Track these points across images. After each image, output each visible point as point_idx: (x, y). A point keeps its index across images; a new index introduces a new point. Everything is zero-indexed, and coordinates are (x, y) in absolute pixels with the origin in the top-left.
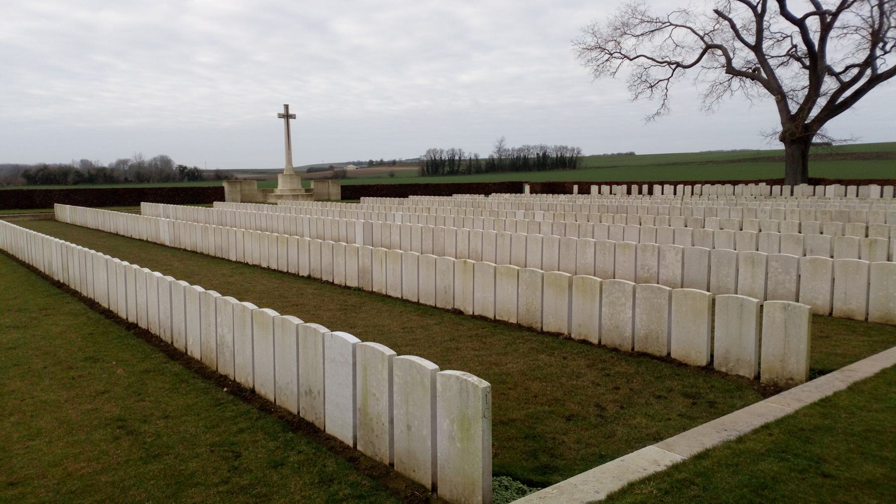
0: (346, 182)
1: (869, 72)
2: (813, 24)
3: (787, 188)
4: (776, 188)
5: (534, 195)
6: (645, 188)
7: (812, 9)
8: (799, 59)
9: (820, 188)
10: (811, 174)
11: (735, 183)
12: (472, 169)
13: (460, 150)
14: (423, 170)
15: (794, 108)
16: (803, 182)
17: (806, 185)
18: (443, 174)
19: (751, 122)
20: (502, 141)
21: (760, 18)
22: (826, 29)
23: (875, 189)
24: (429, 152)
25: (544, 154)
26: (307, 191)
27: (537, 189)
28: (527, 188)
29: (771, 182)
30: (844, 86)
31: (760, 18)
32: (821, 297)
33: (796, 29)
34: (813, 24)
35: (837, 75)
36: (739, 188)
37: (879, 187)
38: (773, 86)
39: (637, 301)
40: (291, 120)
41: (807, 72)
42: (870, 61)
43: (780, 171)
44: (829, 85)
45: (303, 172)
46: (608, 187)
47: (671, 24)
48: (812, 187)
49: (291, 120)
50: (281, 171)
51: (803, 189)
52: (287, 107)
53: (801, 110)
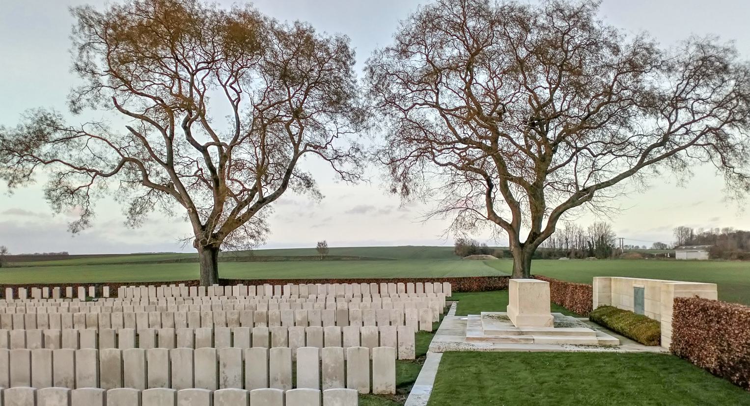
0: (502, 314)
1: (256, 198)
2: (213, 150)
3: (202, 288)
4: (193, 289)
6: (69, 291)
7: (212, 140)
8: (205, 181)
9: (228, 288)
10: (531, 273)
11: (157, 284)
16: (215, 282)
19: (170, 230)
21: (170, 139)
22: (224, 157)
23: (268, 288)
29: (189, 284)
31: (170, 139)
34: (213, 150)
35: (235, 196)
36: (162, 289)
38: (183, 198)
42: (257, 188)
43: (196, 272)
44: (230, 206)
47: (86, 134)
51: (215, 288)
53: (209, 222)
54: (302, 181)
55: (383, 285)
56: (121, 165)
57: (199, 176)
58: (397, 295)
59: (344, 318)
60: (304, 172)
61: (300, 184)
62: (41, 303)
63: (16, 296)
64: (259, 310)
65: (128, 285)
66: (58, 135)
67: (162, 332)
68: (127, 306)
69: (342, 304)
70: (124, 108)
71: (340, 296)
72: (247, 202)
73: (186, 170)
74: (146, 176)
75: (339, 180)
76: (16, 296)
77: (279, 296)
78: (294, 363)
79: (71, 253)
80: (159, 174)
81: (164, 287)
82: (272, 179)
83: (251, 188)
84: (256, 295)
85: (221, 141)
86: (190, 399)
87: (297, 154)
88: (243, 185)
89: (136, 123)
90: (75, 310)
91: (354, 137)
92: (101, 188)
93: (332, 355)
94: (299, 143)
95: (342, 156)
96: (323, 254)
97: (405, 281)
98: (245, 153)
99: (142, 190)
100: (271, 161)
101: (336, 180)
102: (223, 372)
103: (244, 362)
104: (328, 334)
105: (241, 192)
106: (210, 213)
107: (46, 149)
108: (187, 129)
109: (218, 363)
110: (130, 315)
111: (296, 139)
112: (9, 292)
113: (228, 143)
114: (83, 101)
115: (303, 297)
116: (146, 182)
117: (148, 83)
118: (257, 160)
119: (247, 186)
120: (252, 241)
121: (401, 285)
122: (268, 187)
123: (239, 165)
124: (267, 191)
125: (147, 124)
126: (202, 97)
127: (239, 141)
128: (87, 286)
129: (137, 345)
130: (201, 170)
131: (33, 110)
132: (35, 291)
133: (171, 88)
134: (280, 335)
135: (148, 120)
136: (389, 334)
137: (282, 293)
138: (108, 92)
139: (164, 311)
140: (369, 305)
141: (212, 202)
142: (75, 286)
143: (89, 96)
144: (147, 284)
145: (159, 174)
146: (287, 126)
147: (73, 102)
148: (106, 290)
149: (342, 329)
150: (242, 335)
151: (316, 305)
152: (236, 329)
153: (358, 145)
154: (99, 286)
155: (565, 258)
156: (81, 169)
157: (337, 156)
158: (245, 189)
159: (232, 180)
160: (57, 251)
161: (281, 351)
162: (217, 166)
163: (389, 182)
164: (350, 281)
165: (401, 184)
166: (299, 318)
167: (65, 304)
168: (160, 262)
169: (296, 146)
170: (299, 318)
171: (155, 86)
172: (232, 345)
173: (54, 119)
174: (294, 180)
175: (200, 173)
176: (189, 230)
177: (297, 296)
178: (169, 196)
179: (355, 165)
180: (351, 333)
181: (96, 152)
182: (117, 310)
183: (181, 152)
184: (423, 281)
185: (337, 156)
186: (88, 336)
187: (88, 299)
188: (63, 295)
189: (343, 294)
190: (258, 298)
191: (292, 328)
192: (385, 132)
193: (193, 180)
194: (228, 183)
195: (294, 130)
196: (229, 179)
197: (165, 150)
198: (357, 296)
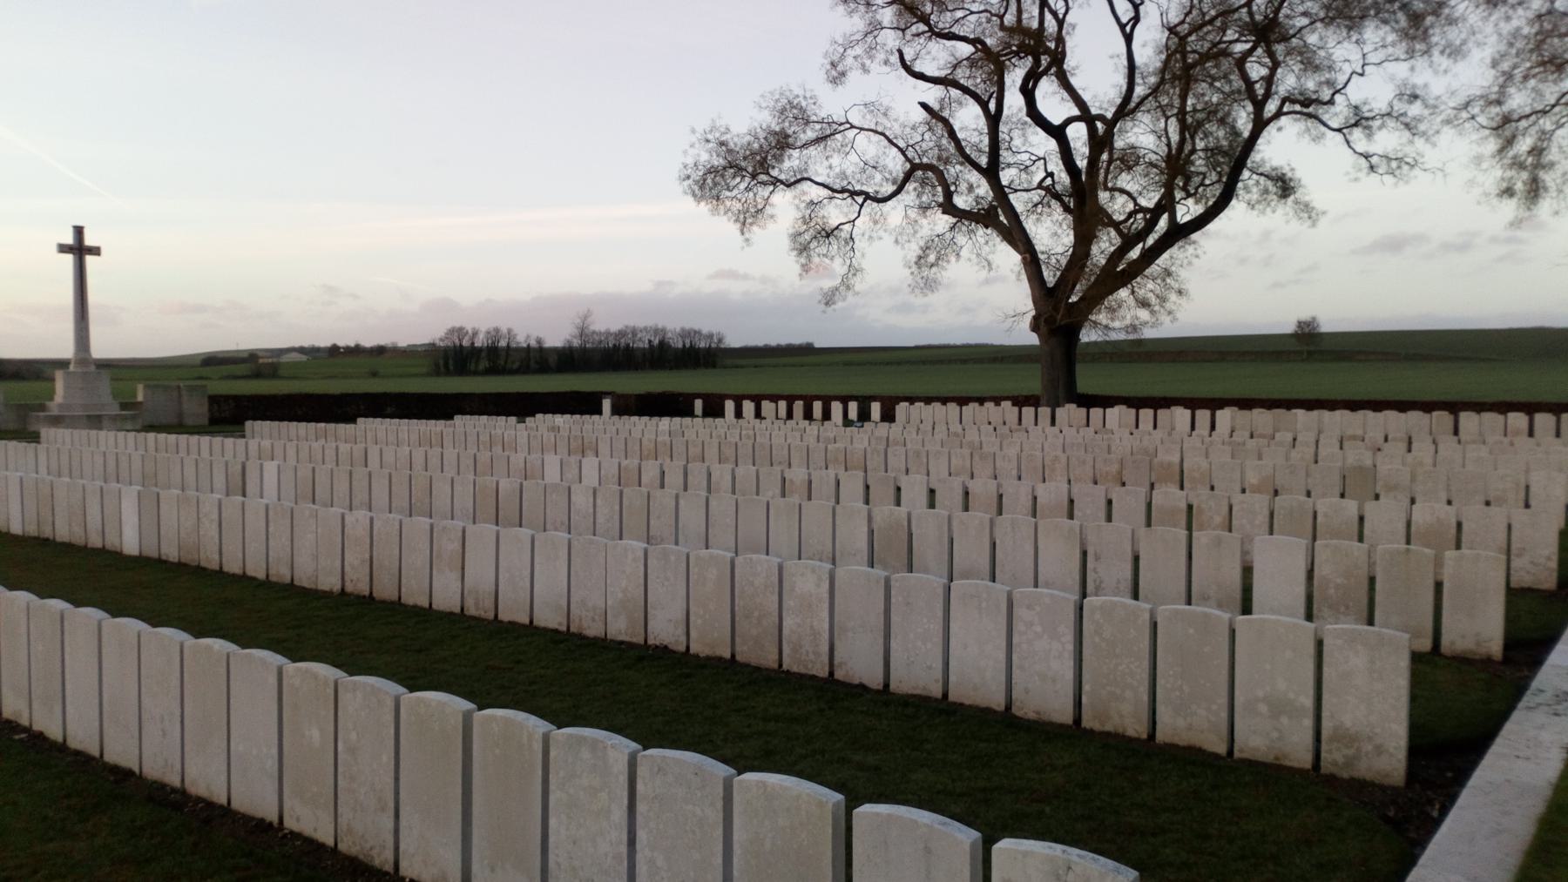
1: (1163, 223)
2: (1078, 134)
3: (1045, 411)
4: (1028, 412)
5: (616, 418)
6: (817, 407)
7: (1076, 112)
9: (1096, 412)
11: (962, 401)
12: (533, 365)
13: (509, 331)
14: (437, 365)
15: (1050, 277)
16: (1070, 401)
17: (1073, 406)
18: (476, 373)
19: (986, 297)
20: (586, 317)
21: (994, 120)
22: (1100, 143)
23: (1181, 415)
24: (452, 331)
25: (662, 343)
26: (124, 406)
27: (627, 406)
28: (607, 404)
29: (1020, 402)
30: (1128, 242)
31: (994, 120)
32: (1128, 694)
33: (1053, 144)
34: (1078, 134)
35: (1117, 226)
37: (1188, 412)
38: (1017, 236)
39: (641, 807)
40: (90, 260)
41: (1070, 218)
43: (1032, 382)
44: (1105, 244)
45: (193, 366)
46: (1151, 412)
47: (852, 127)
48: (1084, 410)
49: (90, 260)
50: (62, 364)
52: (79, 231)
53: (1061, 281)
54: (1269, 183)
55: (1468, 420)
56: (908, 177)
57: (1047, 189)
58: (1506, 440)
59: (1358, 484)
60: (1275, 163)
61: (1266, 191)
62: (776, 426)
63: (739, 414)
64: (1163, 457)
65: (911, 400)
66: (810, 134)
67: (975, 487)
68: (911, 435)
69: (1357, 455)
70: (917, 68)
71: (1354, 438)
72: (1141, 235)
73: (1024, 175)
74: (948, 195)
75: (1362, 175)
76: (739, 414)
77: (1206, 432)
78: (1247, 571)
79: (819, 343)
80: (972, 190)
81: (973, 406)
82: (1202, 184)
83: (1151, 205)
84: (1155, 427)
85: (1094, 111)
86: (1038, 609)
87: (1260, 124)
88: (1134, 200)
89: (933, 94)
90: (828, 441)
91: (1401, 69)
92: (876, 222)
93: (1339, 561)
94: (1268, 95)
95: (1373, 118)
96: (1309, 344)
97: (1530, 408)
98: (1143, 136)
99: (943, 221)
100: (1200, 145)
101: (1352, 176)
102: (1095, 570)
103: (1136, 559)
104: (1326, 515)
105: (1130, 215)
106: (1064, 262)
107: (792, 162)
108: (1028, 92)
109: (1084, 554)
110: (918, 454)
111: (1260, 90)
112: (729, 406)
113: (1109, 115)
114: (849, 61)
115: (1262, 436)
116: (948, 207)
117: (960, 14)
118: (1169, 145)
119: (1143, 202)
120: (1144, 314)
121: (1518, 420)
122: (1190, 201)
123: (1129, 160)
124: (1187, 210)
125: (955, 93)
126: (1061, 23)
127: (1133, 105)
128: (845, 400)
129: (932, 505)
131: (772, 93)
132: (767, 406)
133: (1001, 17)
134: (1211, 508)
135: (956, 84)
136: (1485, 525)
137: (1213, 427)
138: (890, 39)
139: (976, 450)
140: (1428, 460)
141: (1068, 238)
142: (827, 402)
143: (858, 50)
144: (944, 401)
145: (972, 190)
146: (1241, 62)
147: (833, 65)
148: (876, 409)
149: (1361, 508)
150: (1130, 502)
151: (1293, 454)
152: (1117, 494)
153: (1414, 86)
154: (864, 404)
156: (843, 191)
157: (1360, 120)
158: (1139, 209)
159: (1113, 190)
160: (797, 340)
161: (1218, 542)
162: (1082, 163)
163: (1494, 175)
164: (1377, 406)
165: (1525, 175)
166: (1252, 479)
167: (812, 429)
168: (964, 362)
169: (1259, 106)
170: (1252, 479)
171: (973, 18)
172: (1109, 519)
173: (804, 104)
174: (1251, 182)
175: (1049, 181)
177: (1247, 434)
178: (989, 231)
179: (1407, 134)
180: (1385, 516)
181: (867, 158)
182: (897, 444)
183: (1017, 142)
185: (1360, 120)
186: (852, 486)
187: (847, 422)
188: (808, 415)
189: (1359, 432)
190: (1158, 434)
191: (1238, 498)
192: (1488, 53)
193: (1036, 196)
194: (1103, 196)
195: (1256, 71)
196: (1106, 188)
197: (986, 140)
198: (1395, 439)
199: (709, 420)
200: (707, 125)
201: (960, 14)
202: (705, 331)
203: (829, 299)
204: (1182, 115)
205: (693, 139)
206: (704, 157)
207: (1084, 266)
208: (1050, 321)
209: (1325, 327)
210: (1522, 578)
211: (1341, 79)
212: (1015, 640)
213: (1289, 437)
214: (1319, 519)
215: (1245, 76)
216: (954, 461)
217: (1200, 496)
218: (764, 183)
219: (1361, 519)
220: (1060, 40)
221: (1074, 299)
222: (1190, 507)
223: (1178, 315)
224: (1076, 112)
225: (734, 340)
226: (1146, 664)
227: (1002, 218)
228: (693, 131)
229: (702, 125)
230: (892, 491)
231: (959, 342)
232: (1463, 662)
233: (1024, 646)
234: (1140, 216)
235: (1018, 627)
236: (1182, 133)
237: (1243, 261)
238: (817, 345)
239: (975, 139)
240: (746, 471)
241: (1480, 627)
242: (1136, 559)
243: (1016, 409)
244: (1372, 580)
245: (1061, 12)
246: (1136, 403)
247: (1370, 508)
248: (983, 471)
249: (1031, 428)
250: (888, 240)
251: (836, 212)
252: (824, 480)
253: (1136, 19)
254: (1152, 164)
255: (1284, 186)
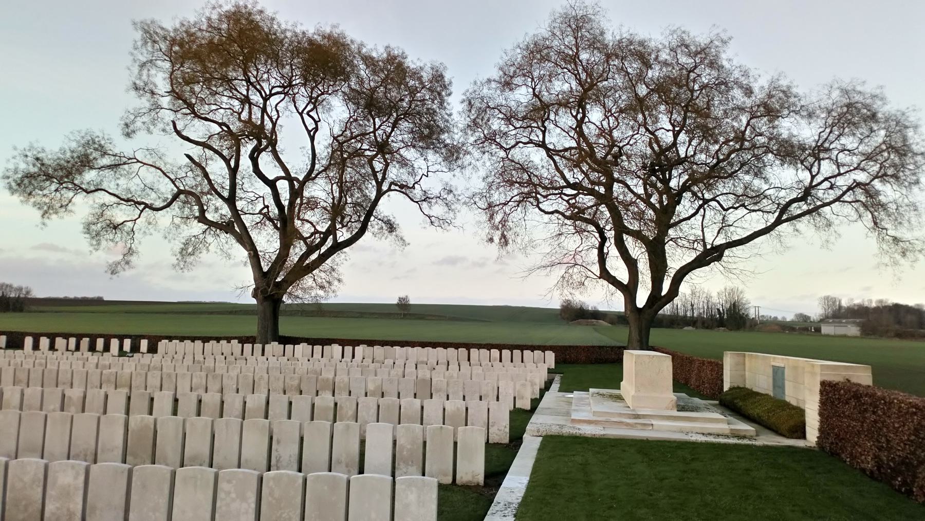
1: (329, 242)
2: (283, 187)
3: (258, 346)
4: (248, 347)
6: (100, 343)
8: (270, 220)
9: (289, 347)
10: (650, 344)
11: (205, 340)
19: (226, 276)
21: (233, 172)
22: (296, 193)
23: (337, 348)
29: (243, 340)
30: (311, 249)
31: (233, 172)
33: (267, 190)
34: (283, 187)
35: (305, 239)
38: (245, 239)
42: (331, 231)
43: (252, 327)
44: (297, 251)
46: (351, 348)
47: (138, 161)
51: (274, 347)
54: (383, 225)
56: (175, 197)
57: (264, 215)
61: (382, 228)
63: (36, 347)
65: (170, 338)
66: (106, 161)
67: (206, 398)
69: (424, 373)
70: (184, 133)
71: (422, 362)
73: (250, 206)
74: (202, 212)
76: (36, 347)
78: (363, 443)
80: (218, 210)
81: (213, 343)
85: (293, 175)
86: (234, 482)
88: (314, 227)
90: (104, 367)
91: (447, 177)
92: (150, 223)
97: (500, 347)
98: (319, 190)
99: (197, 228)
100: (349, 200)
103: (302, 439)
104: (405, 408)
105: (312, 234)
106: (274, 257)
109: (271, 438)
110: (169, 375)
111: (380, 176)
112: (29, 341)
113: (301, 179)
114: (139, 124)
115: (377, 362)
116: (202, 219)
117: (214, 107)
118: (333, 199)
119: (319, 228)
120: (321, 293)
121: (495, 353)
122: (344, 230)
123: (312, 204)
124: (343, 235)
125: (209, 153)
126: (274, 124)
127: (315, 172)
128: (121, 338)
129: (175, 413)
130: (267, 207)
132: (60, 342)
133: (240, 114)
134: (347, 407)
136: (478, 410)
137: (353, 357)
138: (168, 116)
140: (455, 375)
141: (277, 245)
142: (108, 340)
143: (146, 118)
145: (218, 210)
146: (371, 160)
147: (127, 125)
148: (144, 344)
149: (422, 402)
150: (301, 405)
151: (392, 372)
152: (296, 398)
155: (690, 328)
156: (128, 200)
158: (316, 232)
159: (303, 220)
162: (286, 203)
163: (486, 229)
164: (434, 345)
165: (499, 233)
166: (371, 387)
167: (93, 358)
169: (379, 184)
170: (371, 387)
171: (222, 111)
172: (289, 418)
173: (103, 142)
174: (374, 223)
175: (265, 210)
176: (248, 277)
177: (371, 361)
178: (228, 235)
179: (446, 209)
180: (433, 408)
181: (147, 182)
183: (246, 186)
184: (522, 348)
186: (117, 399)
187: (122, 353)
188: (92, 348)
193: (258, 218)
194: (298, 223)
195: (378, 166)
196: (299, 219)
197: (228, 182)
199: (10, 352)
200: (26, 145)
201: (214, 107)
202: (15, 285)
203: (113, 270)
204: (341, 184)
205: (15, 153)
206: (22, 166)
207: (286, 260)
208: (264, 292)
209: (412, 302)
210: (494, 439)
211: (418, 178)
212: (218, 504)
213: (392, 362)
214: (402, 410)
215: (373, 168)
216: (194, 380)
217: (342, 397)
218: (69, 189)
219: (422, 408)
220: (273, 130)
221: (279, 279)
222: (336, 404)
223: (338, 293)
224: (283, 174)
225: (39, 292)
226: (299, 511)
227: (237, 229)
228: (15, 149)
229: (23, 145)
230: (146, 403)
231: (207, 301)
232: (467, 487)
233: (224, 508)
234: (317, 235)
235: (221, 495)
236: (340, 193)
237: (380, 264)
238: (105, 299)
239: (220, 181)
240: (33, 392)
241: (473, 469)
242: (302, 439)
243: (240, 345)
244: (425, 443)
245: (274, 118)
246: (312, 342)
247: (427, 403)
248: (214, 386)
249: (249, 357)
250: (158, 236)
251: (121, 214)
252: (95, 396)
253: (316, 129)
254: (325, 208)
255: (391, 227)
